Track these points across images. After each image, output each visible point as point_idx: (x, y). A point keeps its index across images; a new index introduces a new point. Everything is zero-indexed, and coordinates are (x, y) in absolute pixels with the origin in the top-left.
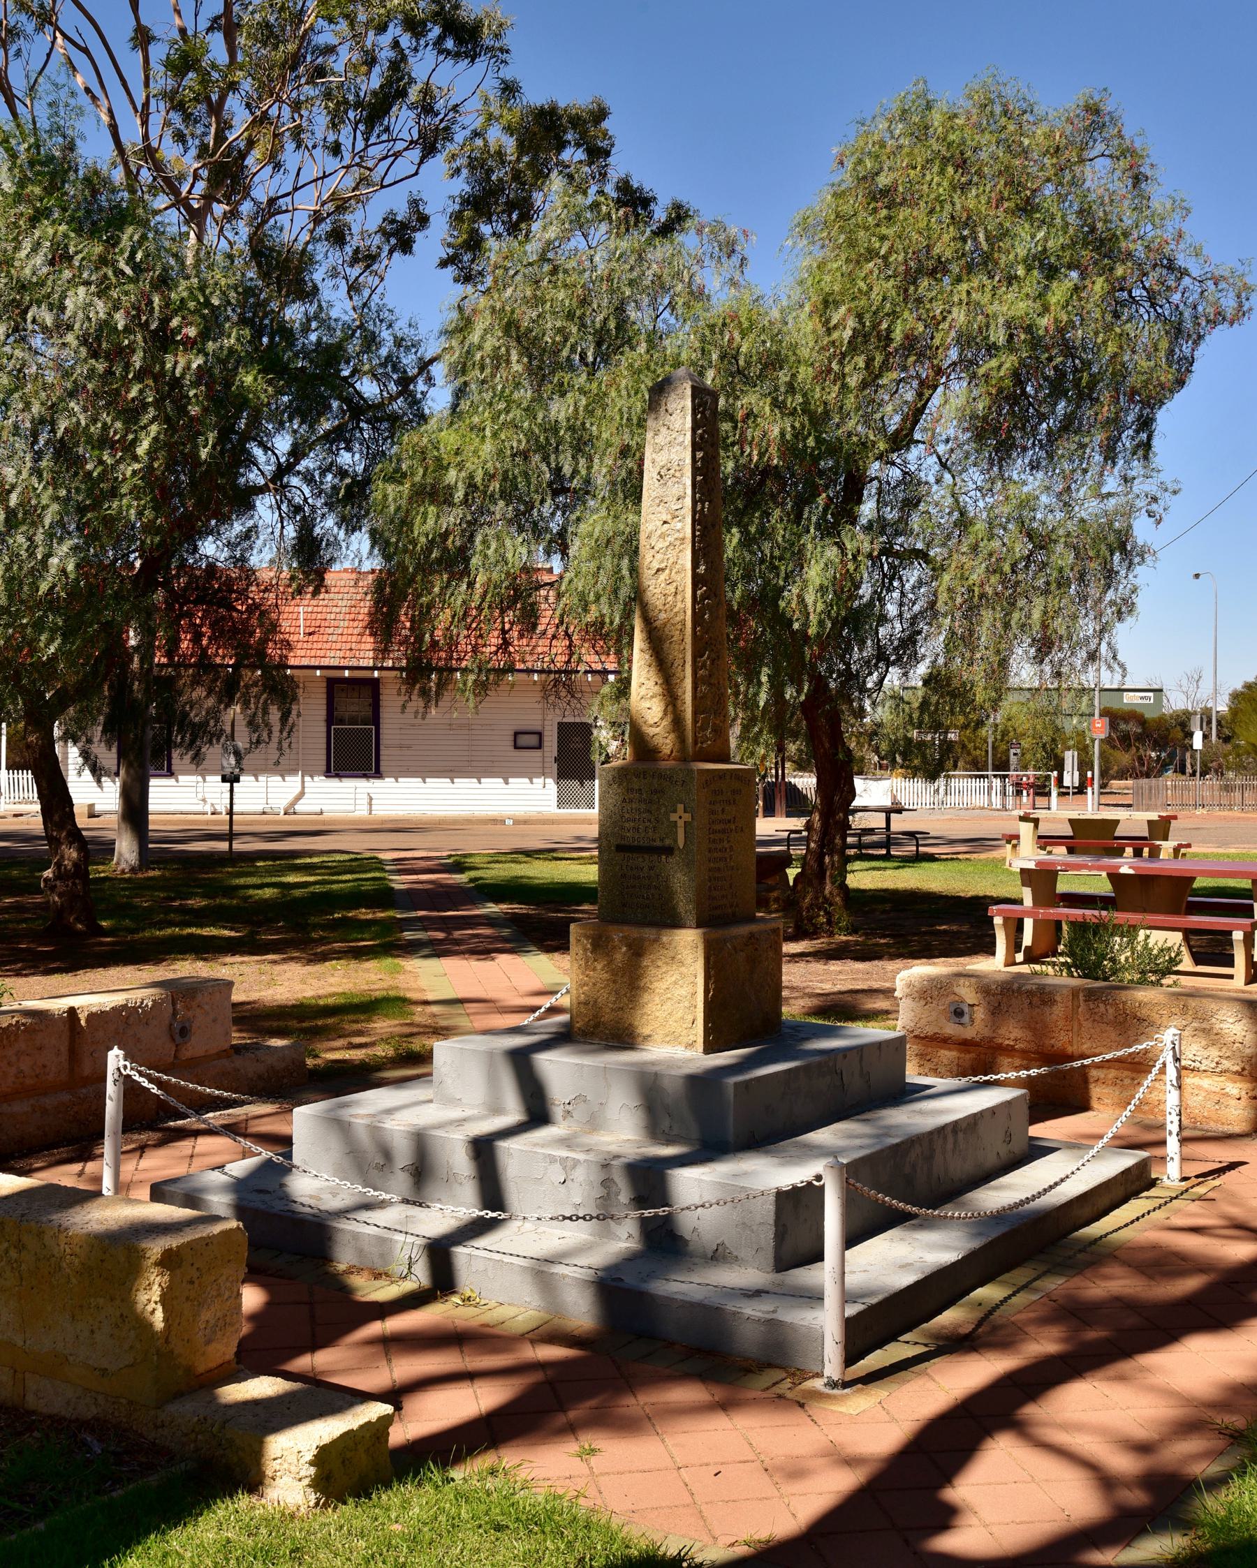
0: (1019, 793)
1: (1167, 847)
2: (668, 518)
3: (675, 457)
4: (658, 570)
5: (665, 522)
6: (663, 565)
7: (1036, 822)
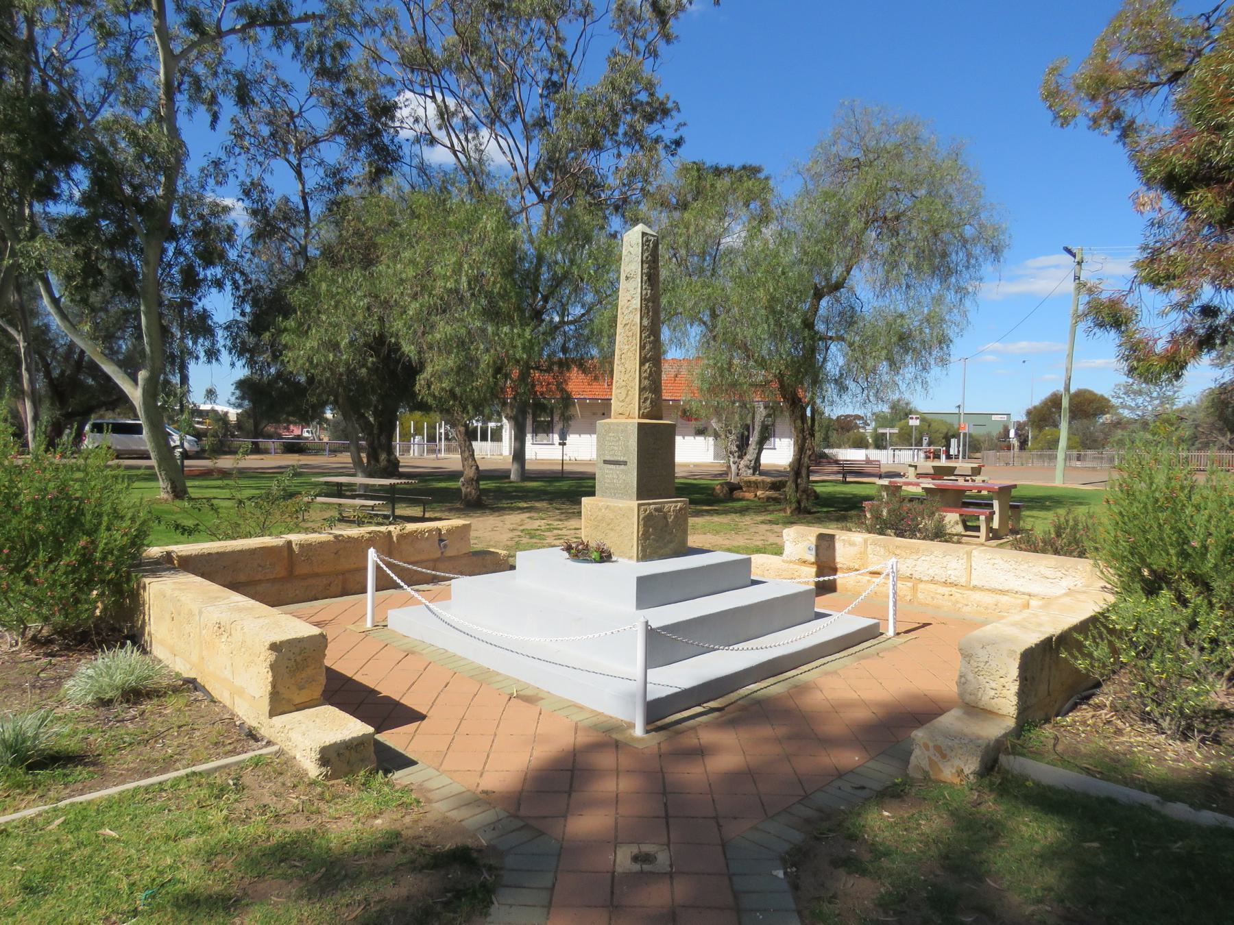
1: (978, 479)
7: (916, 467)
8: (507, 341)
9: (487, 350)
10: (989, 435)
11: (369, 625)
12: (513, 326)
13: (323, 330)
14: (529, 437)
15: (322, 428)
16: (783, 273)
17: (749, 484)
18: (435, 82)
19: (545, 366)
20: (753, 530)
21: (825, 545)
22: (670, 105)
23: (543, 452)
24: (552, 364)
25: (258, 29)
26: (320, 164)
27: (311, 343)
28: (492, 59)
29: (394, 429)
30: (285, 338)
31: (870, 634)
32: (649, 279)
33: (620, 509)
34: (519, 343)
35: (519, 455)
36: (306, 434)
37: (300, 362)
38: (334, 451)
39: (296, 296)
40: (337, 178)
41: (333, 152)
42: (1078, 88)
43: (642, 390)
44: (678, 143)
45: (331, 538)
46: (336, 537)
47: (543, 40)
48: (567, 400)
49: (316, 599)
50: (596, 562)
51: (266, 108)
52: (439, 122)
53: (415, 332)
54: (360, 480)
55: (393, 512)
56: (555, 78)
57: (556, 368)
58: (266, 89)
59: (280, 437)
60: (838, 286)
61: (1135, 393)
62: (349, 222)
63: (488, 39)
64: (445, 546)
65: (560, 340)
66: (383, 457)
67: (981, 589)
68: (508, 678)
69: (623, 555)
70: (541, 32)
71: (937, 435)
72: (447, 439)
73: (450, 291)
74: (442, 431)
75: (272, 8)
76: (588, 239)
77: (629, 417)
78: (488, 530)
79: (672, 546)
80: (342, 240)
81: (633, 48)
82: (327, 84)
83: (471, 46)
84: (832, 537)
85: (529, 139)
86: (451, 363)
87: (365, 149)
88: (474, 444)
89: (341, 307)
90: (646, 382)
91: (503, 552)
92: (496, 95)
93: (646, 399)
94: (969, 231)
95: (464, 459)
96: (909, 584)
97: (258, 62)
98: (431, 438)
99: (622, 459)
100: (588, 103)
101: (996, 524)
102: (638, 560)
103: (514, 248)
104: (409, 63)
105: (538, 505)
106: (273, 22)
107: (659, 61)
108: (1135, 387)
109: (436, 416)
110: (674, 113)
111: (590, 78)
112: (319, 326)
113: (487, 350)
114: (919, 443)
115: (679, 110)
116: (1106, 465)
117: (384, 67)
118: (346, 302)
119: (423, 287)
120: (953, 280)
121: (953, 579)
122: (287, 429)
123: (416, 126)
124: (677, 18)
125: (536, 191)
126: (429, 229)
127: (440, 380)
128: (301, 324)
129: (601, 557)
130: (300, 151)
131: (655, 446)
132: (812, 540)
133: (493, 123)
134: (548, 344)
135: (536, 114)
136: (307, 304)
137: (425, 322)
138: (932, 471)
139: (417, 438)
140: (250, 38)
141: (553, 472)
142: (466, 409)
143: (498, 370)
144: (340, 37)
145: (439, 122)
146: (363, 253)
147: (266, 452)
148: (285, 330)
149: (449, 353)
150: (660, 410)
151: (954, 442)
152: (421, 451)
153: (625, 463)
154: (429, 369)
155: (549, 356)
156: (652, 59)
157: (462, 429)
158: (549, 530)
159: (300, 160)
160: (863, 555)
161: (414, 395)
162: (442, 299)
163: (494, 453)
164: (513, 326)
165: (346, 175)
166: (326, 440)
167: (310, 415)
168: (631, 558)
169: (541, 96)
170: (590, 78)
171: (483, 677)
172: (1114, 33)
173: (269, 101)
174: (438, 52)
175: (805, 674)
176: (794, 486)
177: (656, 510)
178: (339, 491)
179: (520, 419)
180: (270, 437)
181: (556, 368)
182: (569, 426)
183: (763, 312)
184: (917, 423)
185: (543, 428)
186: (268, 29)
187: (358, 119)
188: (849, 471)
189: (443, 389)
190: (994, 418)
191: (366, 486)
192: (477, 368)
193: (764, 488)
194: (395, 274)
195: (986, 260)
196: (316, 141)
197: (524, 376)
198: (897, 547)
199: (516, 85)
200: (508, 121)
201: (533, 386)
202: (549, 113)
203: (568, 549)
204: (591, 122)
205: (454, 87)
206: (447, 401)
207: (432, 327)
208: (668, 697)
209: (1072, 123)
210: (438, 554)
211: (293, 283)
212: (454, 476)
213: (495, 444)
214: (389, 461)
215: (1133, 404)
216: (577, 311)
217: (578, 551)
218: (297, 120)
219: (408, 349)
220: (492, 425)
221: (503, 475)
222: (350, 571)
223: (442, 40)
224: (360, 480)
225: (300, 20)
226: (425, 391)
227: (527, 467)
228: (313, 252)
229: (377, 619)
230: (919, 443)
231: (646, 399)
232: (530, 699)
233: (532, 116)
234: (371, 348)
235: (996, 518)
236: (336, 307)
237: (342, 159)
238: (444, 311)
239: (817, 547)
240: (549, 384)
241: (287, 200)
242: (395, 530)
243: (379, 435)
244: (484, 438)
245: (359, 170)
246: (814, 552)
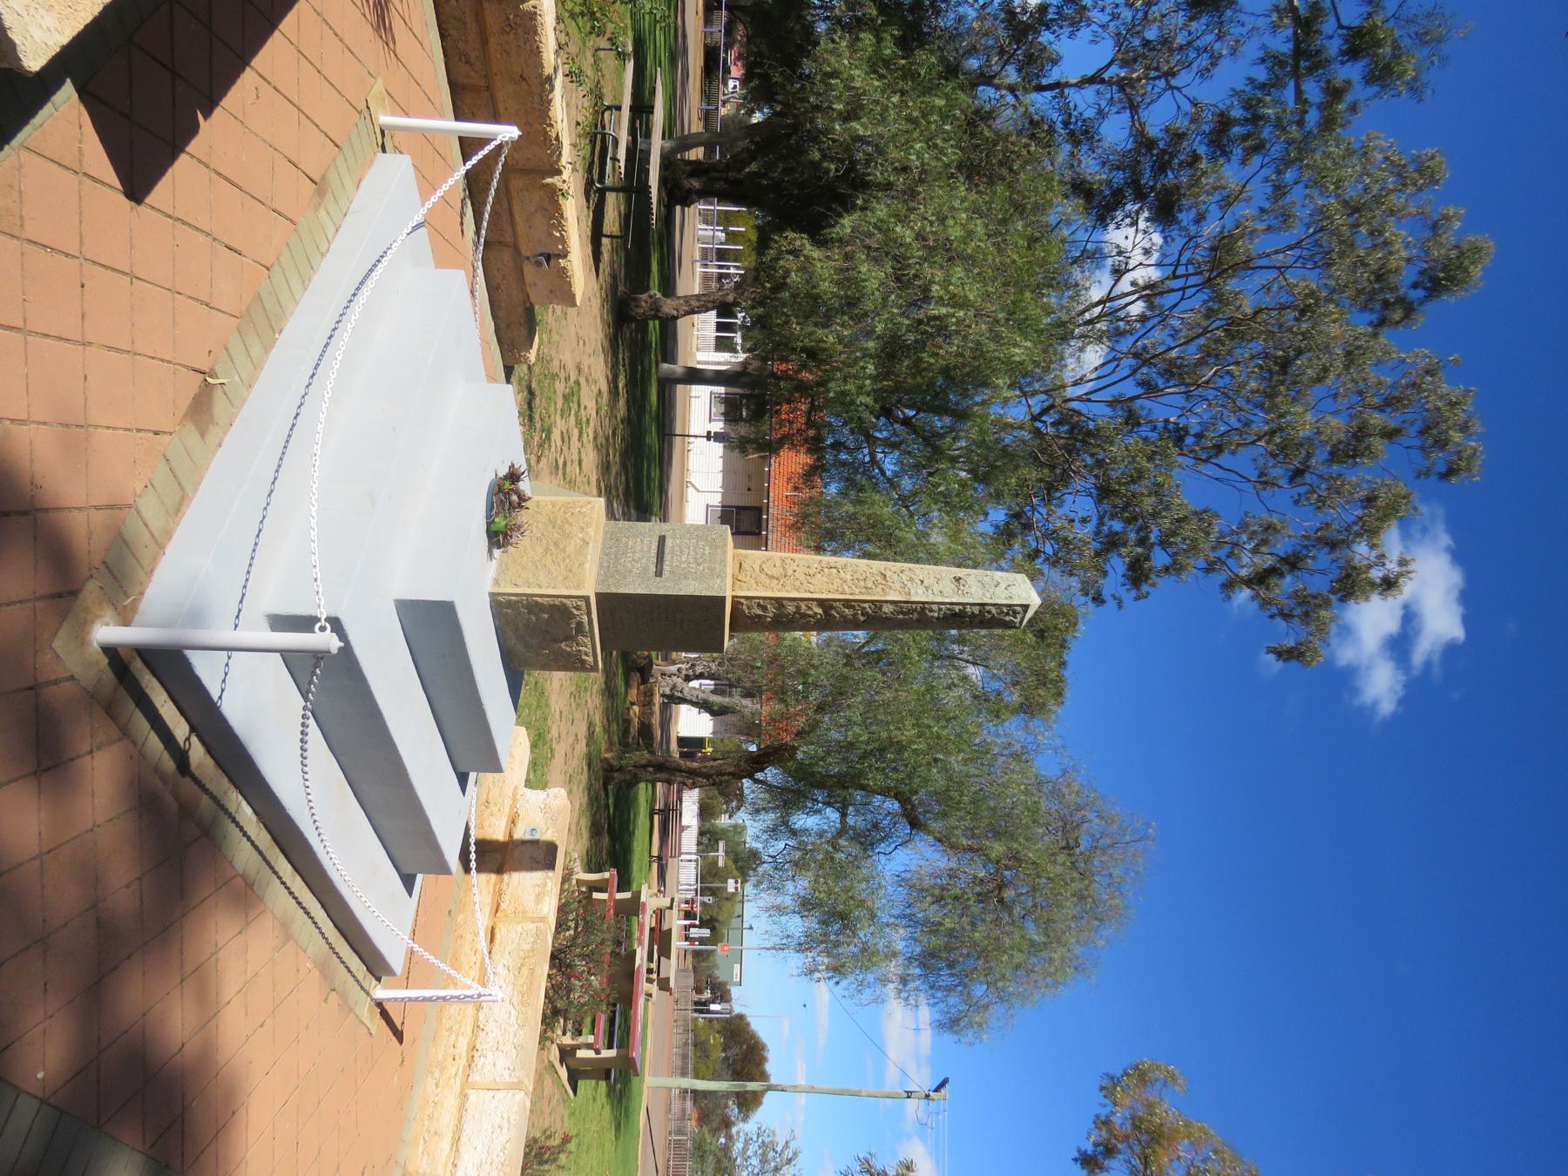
0: (687, 902)
1: (654, 988)
3: (973, 590)
7: (671, 908)
8: (853, 371)
9: (840, 340)
10: (715, 966)
11: (385, 119)
12: (874, 379)
13: (877, 96)
14: (721, 390)
15: (739, 107)
16: (936, 760)
17: (649, 694)
18: (1192, 280)
19: (816, 417)
20: (577, 715)
21: (540, 855)
22: (1145, 588)
23: (699, 409)
24: (818, 428)
25: (1290, 31)
26: (1100, 111)
27: (859, 77)
28: (1217, 356)
29: (736, 203)
30: (867, 38)
31: (376, 965)
32: (955, 615)
33: (581, 565)
34: (850, 387)
35: (695, 376)
36: (731, 83)
37: (832, 59)
38: (707, 117)
39: (925, 60)
40: (1082, 135)
41: (1115, 132)
42: (1150, 1107)
43: (779, 602)
44: (1098, 599)
45: (548, 70)
46: (549, 79)
47: (1238, 425)
48: (769, 448)
49: (442, 36)
50: (489, 525)
51: (1180, 40)
52: (1141, 282)
53: (871, 235)
54: (657, 144)
55: (612, 189)
56: (1189, 440)
57: (812, 433)
58: (1210, 38)
59: (728, 46)
60: (915, 824)
61: (764, 1154)
62: (1027, 146)
63: (1243, 353)
64: (539, 264)
65: (846, 436)
66: (696, 184)
67: (462, 1108)
68: (257, 366)
69: (503, 569)
70: (1247, 424)
71: (713, 918)
72: (721, 276)
73: (926, 289)
74: (732, 271)
75: (1318, 52)
76: (984, 479)
77: (736, 579)
78: (576, 335)
79: (520, 647)
80: (1001, 137)
81: (1220, 543)
82: (1206, 128)
83: (1236, 330)
84: (551, 866)
85: (1110, 404)
86: (825, 286)
87: (1119, 178)
88: (714, 313)
89: (910, 127)
90: (791, 609)
91: (532, 355)
92: (1172, 362)
93: (764, 608)
94: (979, 990)
95: (687, 299)
97: (1244, 31)
98: (722, 255)
99: (666, 568)
100: (1160, 485)
101: (581, 1054)
102: (492, 595)
103: (985, 384)
104: (1223, 244)
105: (622, 402)
106: (1298, 53)
107: (1200, 574)
108: (771, 1154)
109: (751, 260)
110: (1134, 593)
111: (1187, 486)
112: (883, 92)
113: (840, 340)
114: (704, 891)
115: (1137, 599)
116: (673, 1126)
117: (1215, 211)
118: (916, 134)
119: (932, 250)
120: (918, 971)
121: (479, 1061)
122: (739, 58)
123: (1138, 251)
124: (1253, 598)
125: (1045, 411)
126: (1014, 262)
127: (802, 269)
128: (887, 63)
129: (496, 533)
130: (1122, 84)
131: (692, 621)
132: (547, 835)
133: (1136, 355)
134: (845, 424)
135: (1144, 413)
136: (915, 76)
137: (888, 251)
138: (665, 927)
139: (722, 236)
140: (1281, 19)
141: (672, 420)
142: (759, 302)
143: (812, 354)
144: (1276, 150)
145: (1141, 282)
146: (983, 161)
147: (708, 21)
148: (879, 40)
149: (838, 284)
150: (747, 629)
151: (706, 932)
152: (702, 236)
153: (659, 573)
154: (816, 254)
155: (830, 424)
156: (1204, 565)
157: (731, 298)
158: (578, 423)
159: (1109, 83)
160: (522, 916)
161: (780, 230)
162: (916, 276)
163: (700, 342)
164: (874, 379)
165: (1085, 148)
166: (723, 111)
167: (760, 88)
168: (496, 582)
169: (1167, 421)
170: (1187, 486)
171: (260, 320)
172: (1216, 1153)
173: (1189, 43)
174: (1232, 285)
175: (284, 895)
176: (644, 762)
177: (580, 625)
178: (641, 108)
179: (744, 379)
180: (729, 31)
181: (812, 433)
182: (733, 449)
183: (884, 735)
184: (731, 889)
185: (731, 408)
186: (1290, 46)
187: (1161, 167)
188: (668, 816)
189: (787, 273)
190: (737, 967)
191: (646, 154)
192: (816, 325)
193: (642, 714)
194: (952, 208)
195: (942, 1012)
196: (1133, 108)
197: (802, 387)
198: (532, 970)
199: (1183, 389)
200: (1138, 376)
201: (789, 402)
202: (1144, 430)
203: (514, 476)
204: (1136, 488)
205: (1184, 305)
206: (770, 278)
207: (876, 261)
208: (197, 680)
209: (1107, 1101)
210: (526, 252)
211: (943, 59)
212: (668, 286)
213: (713, 342)
214: (690, 191)
215: (750, 1153)
216: (889, 464)
217: (507, 494)
218: (1161, 83)
219: (847, 223)
220: (738, 338)
221: (668, 348)
222: (492, 97)
223: (1246, 293)
224: (657, 144)
225: (1299, 92)
226: (785, 246)
227: (680, 387)
228: (986, 92)
229: (398, 136)
230: (704, 892)
231: (764, 608)
232: (202, 408)
233: (1142, 408)
234: (848, 171)
235: (590, 1054)
236: (909, 119)
237: (1105, 144)
238: (898, 280)
239: (537, 842)
240: (791, 423)
241: (1055, 62)
242: (570, 179)
243: (727, 180)
244: (720, 327)
245: (1091, 168)
246: (528, 837)
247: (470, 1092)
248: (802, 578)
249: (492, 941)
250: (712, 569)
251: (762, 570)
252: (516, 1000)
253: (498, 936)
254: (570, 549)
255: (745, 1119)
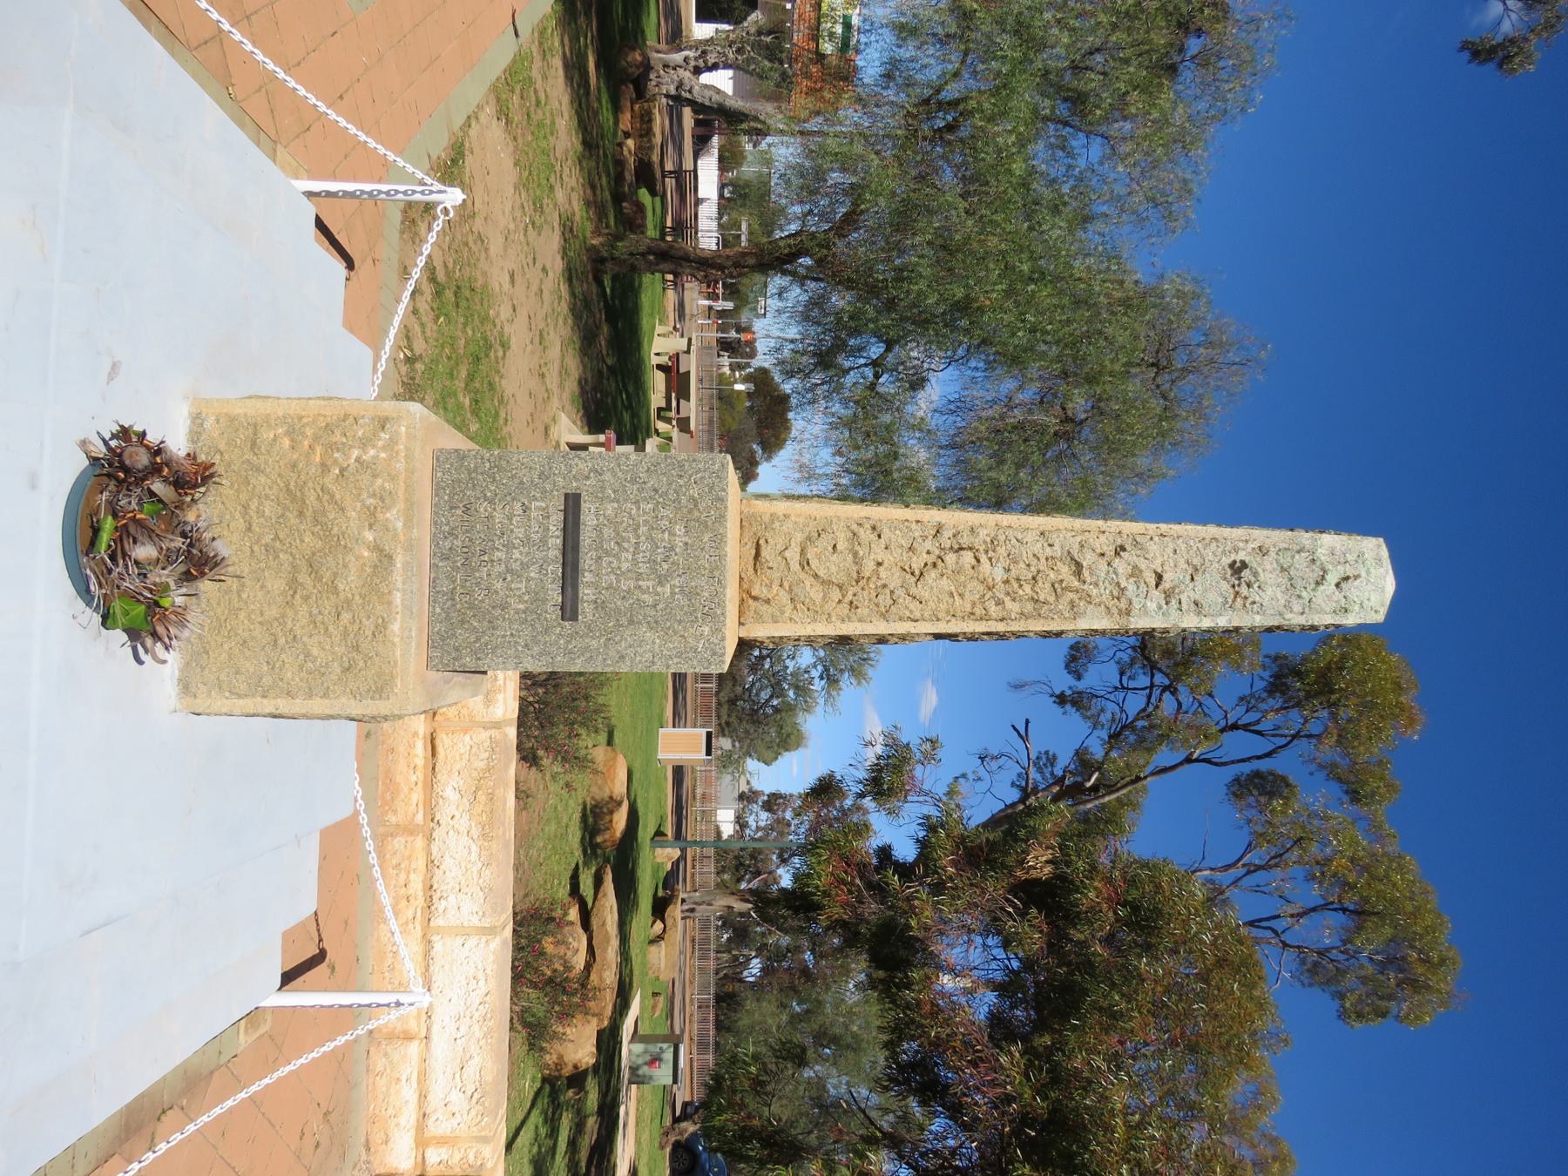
2: (1166, 585)
4: (1079, 565)
5: (1159, 577)
6: (1086, 573)
7: (688, 352)
33: (381, 628)
67: (427, 955)
96: (420, 817)
99: (586, 592)
193: (639, 148)
198: (491, 798)
247: (435, 938)
248: (893, 578)
249: (434, 755)
250: (692, 594)
251: (805, 564)
252: (475, 832)
253: (440, 750)
254: (350, 583)
255: (769, 458)
